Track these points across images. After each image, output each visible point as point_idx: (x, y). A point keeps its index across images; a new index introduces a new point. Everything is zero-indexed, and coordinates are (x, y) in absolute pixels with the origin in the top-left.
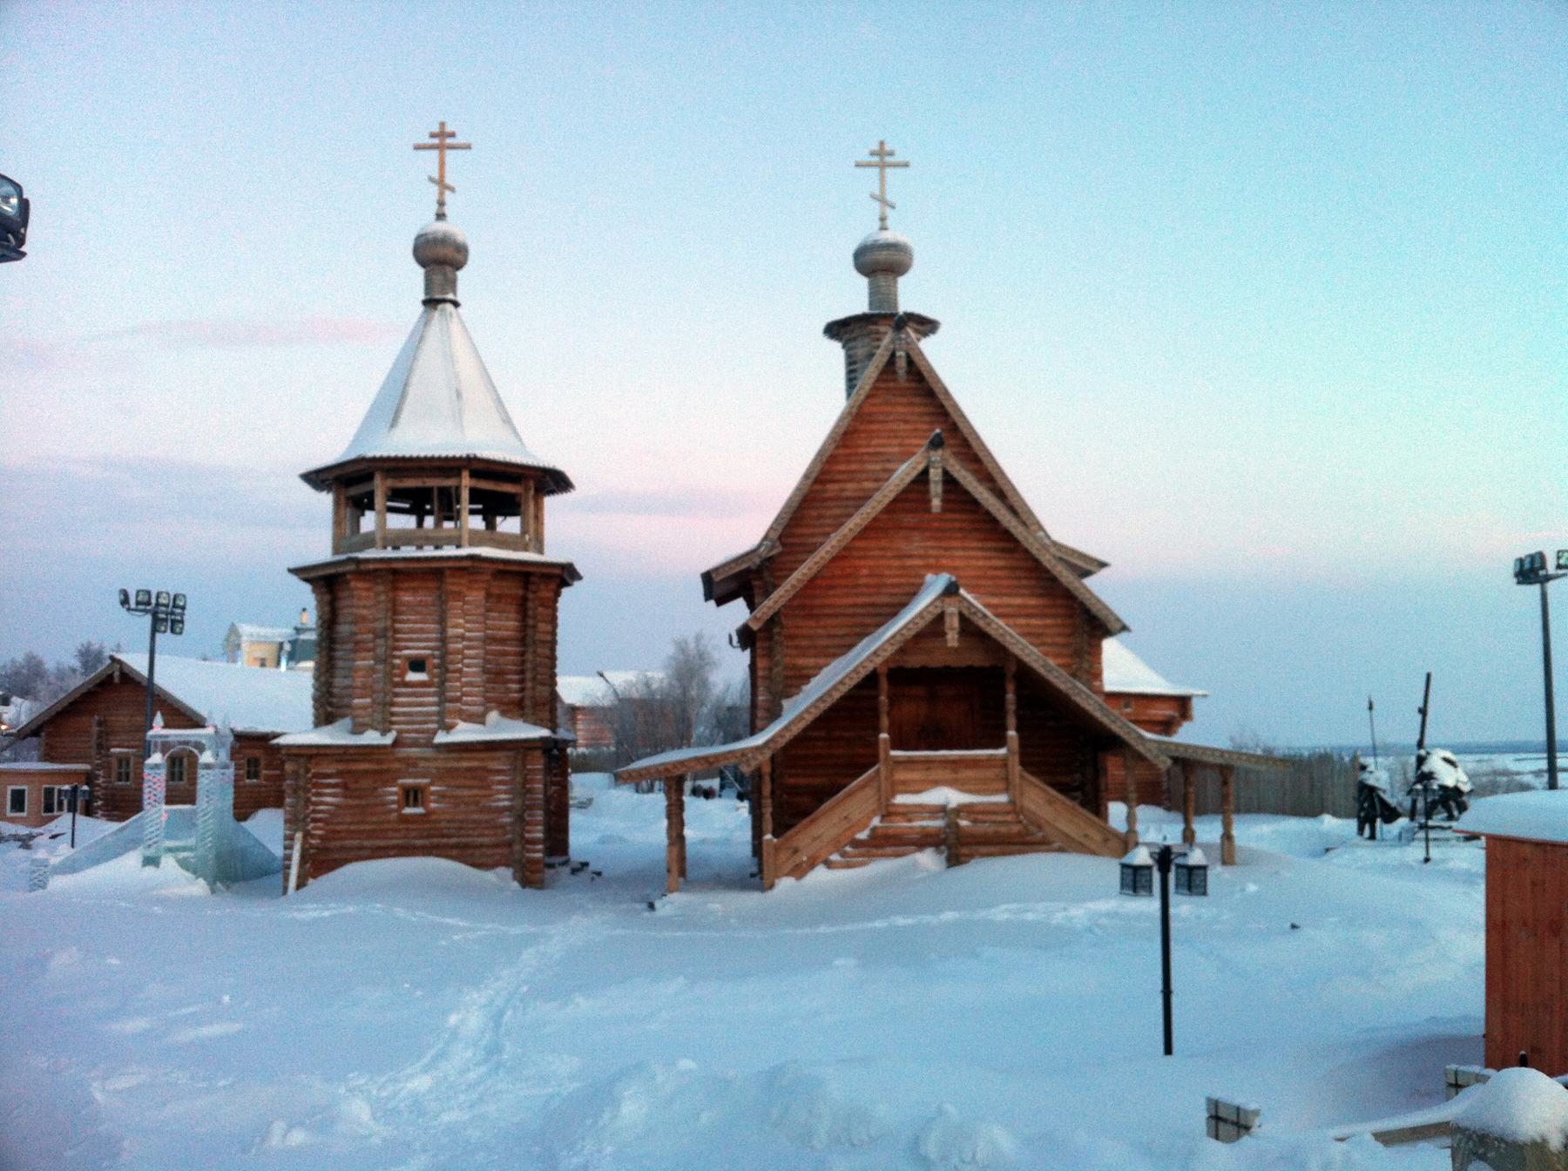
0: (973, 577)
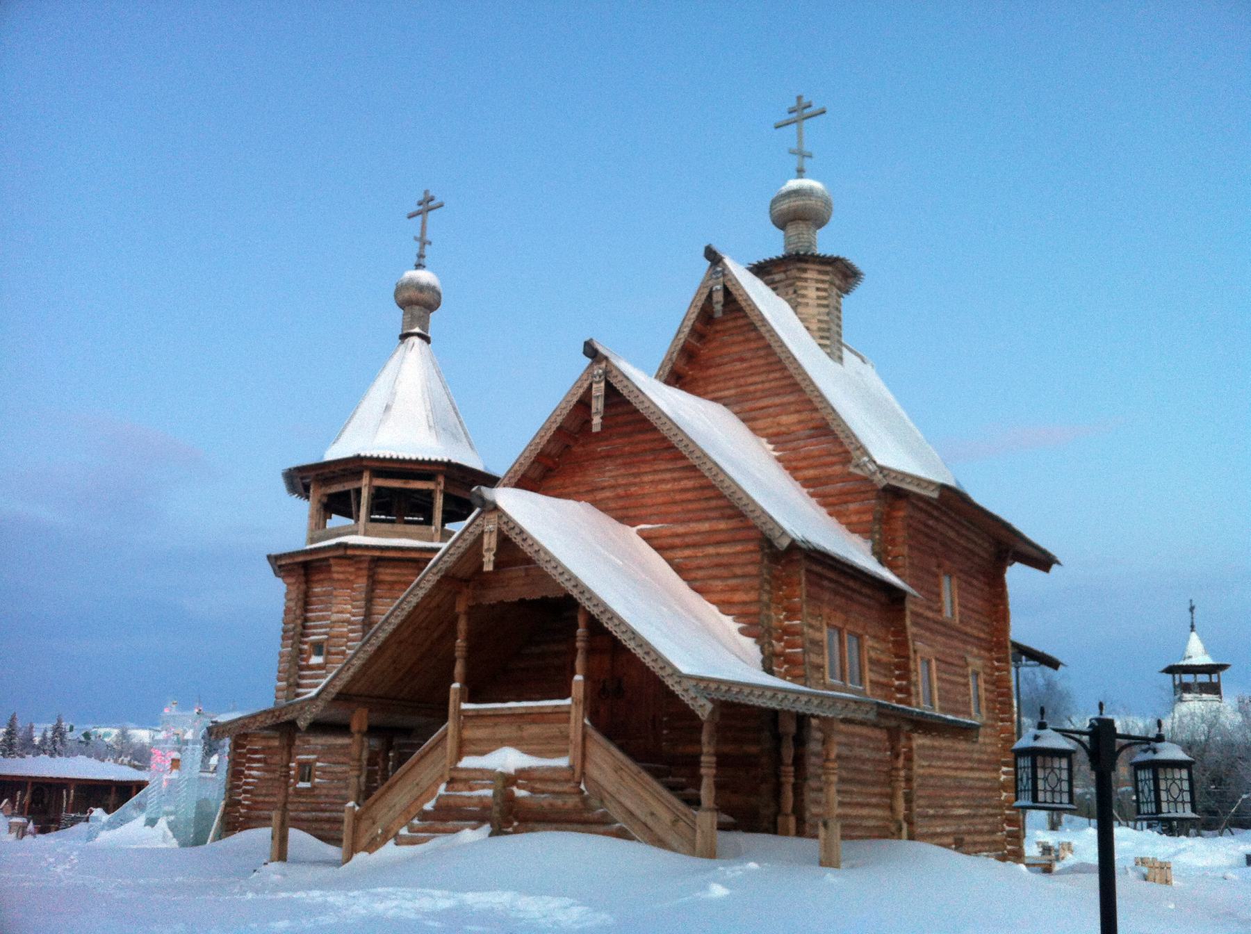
0: (664, 504)
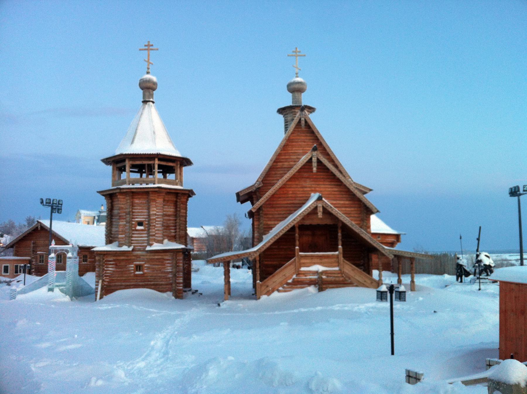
0: (327, 194)
